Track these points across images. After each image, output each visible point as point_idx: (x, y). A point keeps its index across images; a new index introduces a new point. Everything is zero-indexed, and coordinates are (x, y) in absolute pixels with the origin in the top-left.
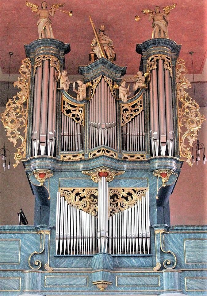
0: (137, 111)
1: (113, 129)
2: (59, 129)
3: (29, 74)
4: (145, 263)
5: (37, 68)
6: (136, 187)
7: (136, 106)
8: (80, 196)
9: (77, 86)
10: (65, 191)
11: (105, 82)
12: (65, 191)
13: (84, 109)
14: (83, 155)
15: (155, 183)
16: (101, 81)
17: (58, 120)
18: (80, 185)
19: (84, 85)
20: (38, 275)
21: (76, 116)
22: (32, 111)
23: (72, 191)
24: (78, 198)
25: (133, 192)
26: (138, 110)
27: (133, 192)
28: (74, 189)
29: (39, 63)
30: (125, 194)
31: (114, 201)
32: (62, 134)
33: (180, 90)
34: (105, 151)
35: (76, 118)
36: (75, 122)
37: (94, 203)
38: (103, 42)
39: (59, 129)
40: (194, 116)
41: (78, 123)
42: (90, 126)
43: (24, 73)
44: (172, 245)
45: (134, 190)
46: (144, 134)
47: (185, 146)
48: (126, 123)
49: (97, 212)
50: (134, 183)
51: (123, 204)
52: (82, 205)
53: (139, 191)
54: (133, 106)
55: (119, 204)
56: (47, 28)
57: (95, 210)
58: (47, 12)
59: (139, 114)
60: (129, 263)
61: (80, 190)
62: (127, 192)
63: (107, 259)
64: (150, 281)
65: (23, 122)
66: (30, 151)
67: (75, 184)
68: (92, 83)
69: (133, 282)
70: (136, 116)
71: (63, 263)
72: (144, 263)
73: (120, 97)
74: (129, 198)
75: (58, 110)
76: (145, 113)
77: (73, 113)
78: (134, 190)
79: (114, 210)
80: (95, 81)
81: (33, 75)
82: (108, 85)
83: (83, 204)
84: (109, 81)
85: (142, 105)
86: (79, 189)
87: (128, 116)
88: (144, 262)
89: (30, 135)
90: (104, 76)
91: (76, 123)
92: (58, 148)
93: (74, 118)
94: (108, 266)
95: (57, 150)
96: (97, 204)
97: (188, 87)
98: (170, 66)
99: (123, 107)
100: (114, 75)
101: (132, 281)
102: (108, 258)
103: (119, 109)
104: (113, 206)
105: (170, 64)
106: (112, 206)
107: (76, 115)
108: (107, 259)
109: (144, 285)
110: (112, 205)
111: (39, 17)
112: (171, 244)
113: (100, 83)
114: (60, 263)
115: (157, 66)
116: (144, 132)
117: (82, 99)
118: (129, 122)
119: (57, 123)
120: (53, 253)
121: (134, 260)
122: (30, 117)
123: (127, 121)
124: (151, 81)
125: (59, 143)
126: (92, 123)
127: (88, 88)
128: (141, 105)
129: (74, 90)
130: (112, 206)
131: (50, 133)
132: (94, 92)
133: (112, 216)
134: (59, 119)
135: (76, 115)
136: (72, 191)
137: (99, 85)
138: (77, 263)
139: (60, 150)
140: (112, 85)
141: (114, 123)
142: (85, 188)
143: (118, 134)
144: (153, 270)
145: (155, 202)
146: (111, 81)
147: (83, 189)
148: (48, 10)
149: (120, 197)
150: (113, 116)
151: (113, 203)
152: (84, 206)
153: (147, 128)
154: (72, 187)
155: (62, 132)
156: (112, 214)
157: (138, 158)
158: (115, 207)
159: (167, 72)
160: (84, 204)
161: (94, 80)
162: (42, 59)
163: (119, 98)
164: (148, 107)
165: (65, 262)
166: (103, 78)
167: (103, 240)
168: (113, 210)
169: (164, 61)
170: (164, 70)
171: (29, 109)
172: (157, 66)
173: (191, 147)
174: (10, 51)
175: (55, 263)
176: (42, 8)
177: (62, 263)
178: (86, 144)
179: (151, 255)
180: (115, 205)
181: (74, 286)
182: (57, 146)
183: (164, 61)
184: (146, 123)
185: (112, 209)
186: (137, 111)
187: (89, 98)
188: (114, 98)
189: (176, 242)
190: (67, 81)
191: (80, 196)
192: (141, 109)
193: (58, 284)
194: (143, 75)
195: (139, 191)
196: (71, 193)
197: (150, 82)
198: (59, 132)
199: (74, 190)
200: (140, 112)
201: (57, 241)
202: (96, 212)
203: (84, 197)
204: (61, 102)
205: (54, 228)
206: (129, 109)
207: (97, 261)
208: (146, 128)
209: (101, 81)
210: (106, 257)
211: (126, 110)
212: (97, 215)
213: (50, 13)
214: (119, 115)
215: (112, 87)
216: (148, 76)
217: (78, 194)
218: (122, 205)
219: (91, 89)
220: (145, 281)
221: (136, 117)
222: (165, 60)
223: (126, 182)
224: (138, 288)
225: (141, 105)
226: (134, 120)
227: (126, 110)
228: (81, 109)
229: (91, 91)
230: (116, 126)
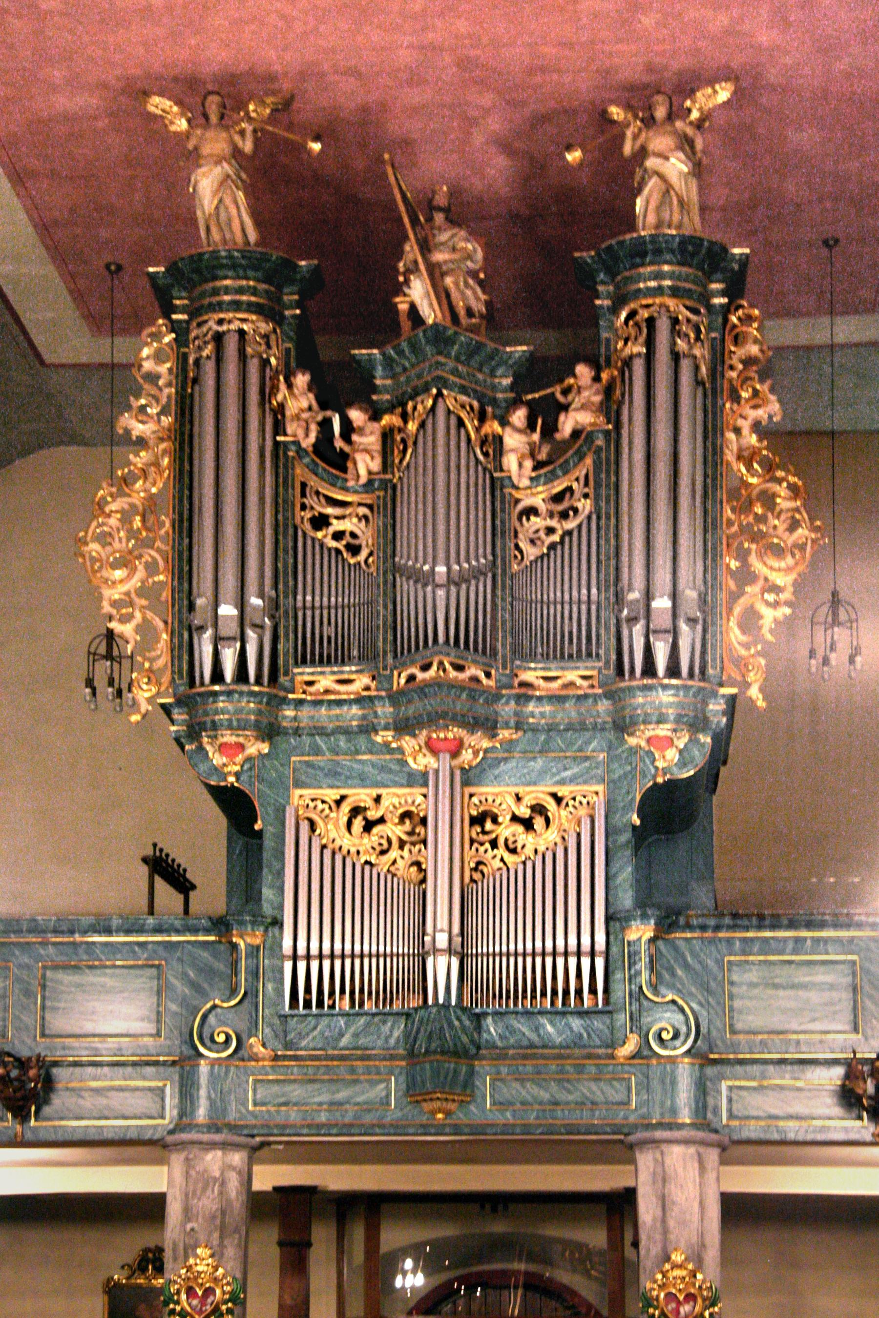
0: (571, 513)
1: (473, 588)
2: (286, 584)
3: (169, 385)
4: (589, 1035)
5: (197, 362)
6: (562, 782)
7: (568, 495)
8: (365, 819)
9: (348, 429)
10: (313, 800)
11: (449, 412)
12: (313, 800)
13: (375, 509)
14: (374, 678)
15: (630, 772)
16: (433, 409)
17: (281, 554)
18: (363, 781)
19: (376, 425)
20: (227, 1072)
21: (348, 539)
22: (186, 524)
23: (339, 802)
24: (358, 823)
25: (551, 805)
26: (576, 511)
27: (551, 805)
28: (343, 792)
29: (206, 343)
30: (524, 812)
31: (484, 832)
32: (299, 604)
33: (737, 431)
34: (447, 666)
35: (348, 547)
36: (343, 560)
37: (414, 838)
38: (439, 256)
39: (286, 584)
40: (785, 526)
41: (355, 565)
42: (397, 576)
43: (152, 378)
44: (684, 976)
45: (554, 796)
46: (594, 597)
47: (743, 638)
48: (531, 562)
49: (425, 871)
50: (554, 770)
51: (515, 842)
52: (373, 848)
53: (574, 799)
54: (557, 498)
55: (501, 842)
56: (228, 201)
57: (418, 864)
58: (224, 135)
59: (580, 526)
60: (533, 1036)
61: (363, 797)
62: (528, 800)
63: (456, 1023)
64: (602, 1091)
65: (158, 563)
66: (185, 667)
67: (348, 778)
68: (405, 417)
69: (545, 1096)
70: (569, 533)
71: (310, 1037)
72: (585, 1035)
73: (505, 468)
74: (539, 822)
75: (280, 517)
76: (603, 522)
77: (337, 525)
78: (554, 796)
79: (485, 865)
80: (415, 408)
81: (184, 388)
82: (461, 423)
83: (375, 845)
84: (463, 406)
85: (590, 490)
86: (362, 796)
87: (537, 535)
88: (582, 1031)
89: (185, 610)
90: (445, 392)
91: (349, 565)
92: (286, 654)
93: (340, 545)
94: (459, 1044)
95: (281, 661)
96: (424, 842)
97: (770, 417)
98: (698, 339)
99: (517, 501)
100: (485, 381)
101: (542, 1093)
102: (458, 1019)
103: (503, 510)
104: (482, 849)
105: (698, 332)
106: (477, 850)
107: (347, 534)
108: (456, 1023)
109: (583, 1103)
110: (475, 845)
111: (194, 158)
112: (679, 972)
113: (431, 417)
114: (301, 1036)
115: (650, 343)
116: (594, 591)
117: (363, 479)
118: (542, 557)
119: (280, 565)
120: (276, 1005)
121: (551, 1023)
122: (180, 544)
123: (531, 552)
124: (627, 402)
125: (287, 635)
126: (403, 562)
127: (387, 436)
128: (586, 490)
129: (339, 444)
130: (477, 850)
131: (256, 601)
132: (410, 451)
133: (475, 882)
134: (286, 551)
135: (347, 534)
136: (339, 802)
137: (429, 422)
138: (356, 1035)
139: (291, 661)
140: (476, 422)
141: (483, 561)
142: (383, 791)
143: (499, 602)
144: (597, 1065)
145: (626, 837)
146: (471, 407)
147: (375, 795)
148: (227, 128)
149: (505, 819)
150: (406, 624)
151: (482, 838)
152: (378, 849)
153: (607, 574)
154: (338, 787)
155: (300, 597)
156: (477, 876)
157: (572, 684)
158: (486, 851)
159: (686, 365)
160: (380, 844)
161: (410, 405)
162: (216, 327)
163: (502, 470)
164: (612, 498)
165: (315, 1033)
166: (440, 400)
167: (442, 960)
168: (479, 863)
169: (675, 321)
170: (676, 357)
171: (177, 517)
172: (650, 343)
173: (765, 642)
174: (108, 258)
175: (282, 1035)
176: (206, 117)
177: (307, 1034)
178: (385, 640)
179: (610, 1008)
180: (487, 845)
181: (347, 1106)
182: (280, 647)
183: (675, 321)
184: (602, 557)
185: (476, 860)
186: (571, 513)
187: (393, 473)
188: (485, 469)
189: (698, 967)
190: (310, 408)
191: (365, 819)
192: (585, 506)
193: (294, 1100)
194: (597, 379)
195: (574, 799)
196: (333, 805)
197: (620, 404)
198: (286, 596)
199: (343, 798)
200: (581, 517)
201: (288, 966)
202: (420, 870)
203: (382, 820)
204: (293, 488)
205: (277, 923)
206: (542, 507)
207: (422, 1030)
208: (602, 576)
209: (433, 409)
210: (453, 1018)
211: (532, 511)
212: (424, 881)
213: (237, 138)
214: (503, 533)
215: (478, 430)
216: (613, 379)
217: (356, 811)
218: (511, 846)
219: (398, 438)
220: (585, 1091)
221: (567, 539)
222: (680, 317)
223: (524, 767)
224: (559, 1113)
225: (586, 490)
226: (559, 547)
227: (532, 511)
228: (362, 511)
229: (401, 447)
230: (490, 575)
